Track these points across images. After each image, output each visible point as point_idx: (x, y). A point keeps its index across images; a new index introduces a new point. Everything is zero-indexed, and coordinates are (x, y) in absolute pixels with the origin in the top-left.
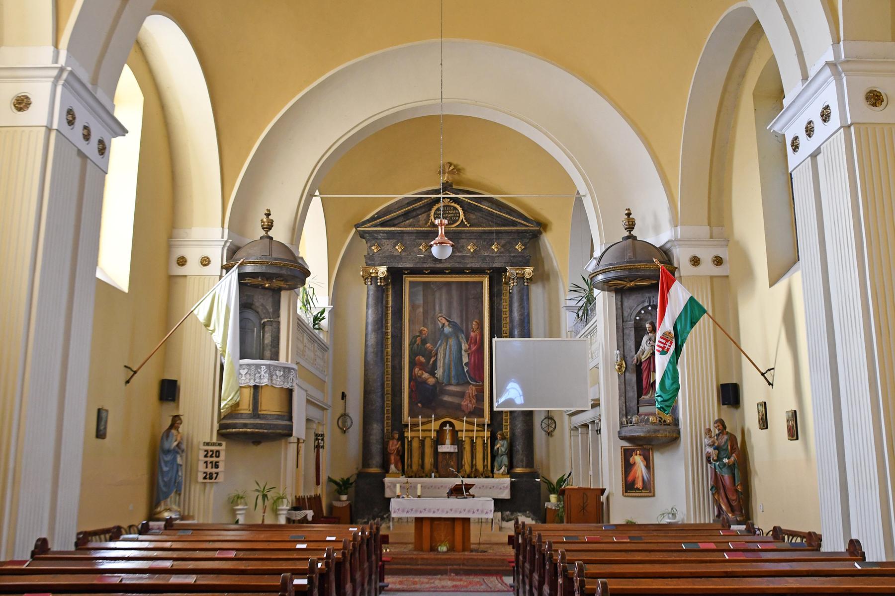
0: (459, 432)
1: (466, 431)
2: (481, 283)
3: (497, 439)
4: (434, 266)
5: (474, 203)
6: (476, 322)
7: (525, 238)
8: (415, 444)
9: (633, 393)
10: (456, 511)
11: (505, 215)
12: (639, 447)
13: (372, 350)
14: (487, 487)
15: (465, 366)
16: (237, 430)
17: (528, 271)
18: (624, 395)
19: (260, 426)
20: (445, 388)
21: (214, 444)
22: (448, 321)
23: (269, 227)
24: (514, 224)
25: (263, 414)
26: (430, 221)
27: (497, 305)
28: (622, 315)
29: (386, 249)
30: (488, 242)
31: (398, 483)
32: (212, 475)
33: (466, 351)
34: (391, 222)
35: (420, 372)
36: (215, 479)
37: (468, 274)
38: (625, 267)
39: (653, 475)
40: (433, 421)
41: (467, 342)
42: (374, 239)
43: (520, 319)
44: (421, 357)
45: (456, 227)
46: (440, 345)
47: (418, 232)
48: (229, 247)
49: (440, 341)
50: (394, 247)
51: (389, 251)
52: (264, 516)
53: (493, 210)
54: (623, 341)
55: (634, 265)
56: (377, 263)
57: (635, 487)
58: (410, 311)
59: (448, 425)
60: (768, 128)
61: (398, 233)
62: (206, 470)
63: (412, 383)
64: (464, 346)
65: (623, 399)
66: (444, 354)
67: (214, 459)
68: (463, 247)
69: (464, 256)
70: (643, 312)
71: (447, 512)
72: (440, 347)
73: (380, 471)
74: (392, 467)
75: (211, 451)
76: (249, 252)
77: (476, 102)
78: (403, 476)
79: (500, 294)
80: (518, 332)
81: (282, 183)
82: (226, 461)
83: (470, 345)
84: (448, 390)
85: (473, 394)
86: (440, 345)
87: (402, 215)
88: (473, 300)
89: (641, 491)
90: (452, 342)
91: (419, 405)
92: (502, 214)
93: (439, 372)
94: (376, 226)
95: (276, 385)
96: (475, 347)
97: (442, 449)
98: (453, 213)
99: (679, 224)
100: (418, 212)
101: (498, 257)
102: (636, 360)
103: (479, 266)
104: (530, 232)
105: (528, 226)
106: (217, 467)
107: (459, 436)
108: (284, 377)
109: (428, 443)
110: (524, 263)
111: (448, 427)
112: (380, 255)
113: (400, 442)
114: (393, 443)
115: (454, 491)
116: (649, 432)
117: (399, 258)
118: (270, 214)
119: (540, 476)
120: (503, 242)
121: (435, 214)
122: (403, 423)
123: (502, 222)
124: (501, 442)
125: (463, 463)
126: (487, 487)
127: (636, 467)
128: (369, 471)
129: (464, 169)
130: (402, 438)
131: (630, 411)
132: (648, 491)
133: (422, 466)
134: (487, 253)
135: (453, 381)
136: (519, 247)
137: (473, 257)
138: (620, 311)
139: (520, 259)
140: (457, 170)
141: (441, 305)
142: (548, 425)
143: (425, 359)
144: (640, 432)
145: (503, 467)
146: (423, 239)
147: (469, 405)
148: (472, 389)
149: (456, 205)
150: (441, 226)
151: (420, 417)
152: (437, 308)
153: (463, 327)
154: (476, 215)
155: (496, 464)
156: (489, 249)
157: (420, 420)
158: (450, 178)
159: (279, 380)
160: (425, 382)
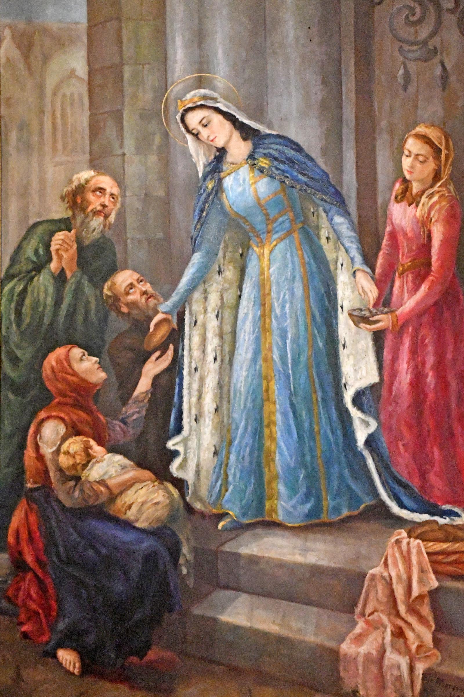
6: (426, 139)
15: (355, 413)
20: (228, 548)
44: (77, 352)
49: (197, 258)
66: (221, 336)
72: (197, 295)
84: (253, 560)
85: (415, 592)
96: (424, 288)
143: (102, 366)
148: (407, 559)
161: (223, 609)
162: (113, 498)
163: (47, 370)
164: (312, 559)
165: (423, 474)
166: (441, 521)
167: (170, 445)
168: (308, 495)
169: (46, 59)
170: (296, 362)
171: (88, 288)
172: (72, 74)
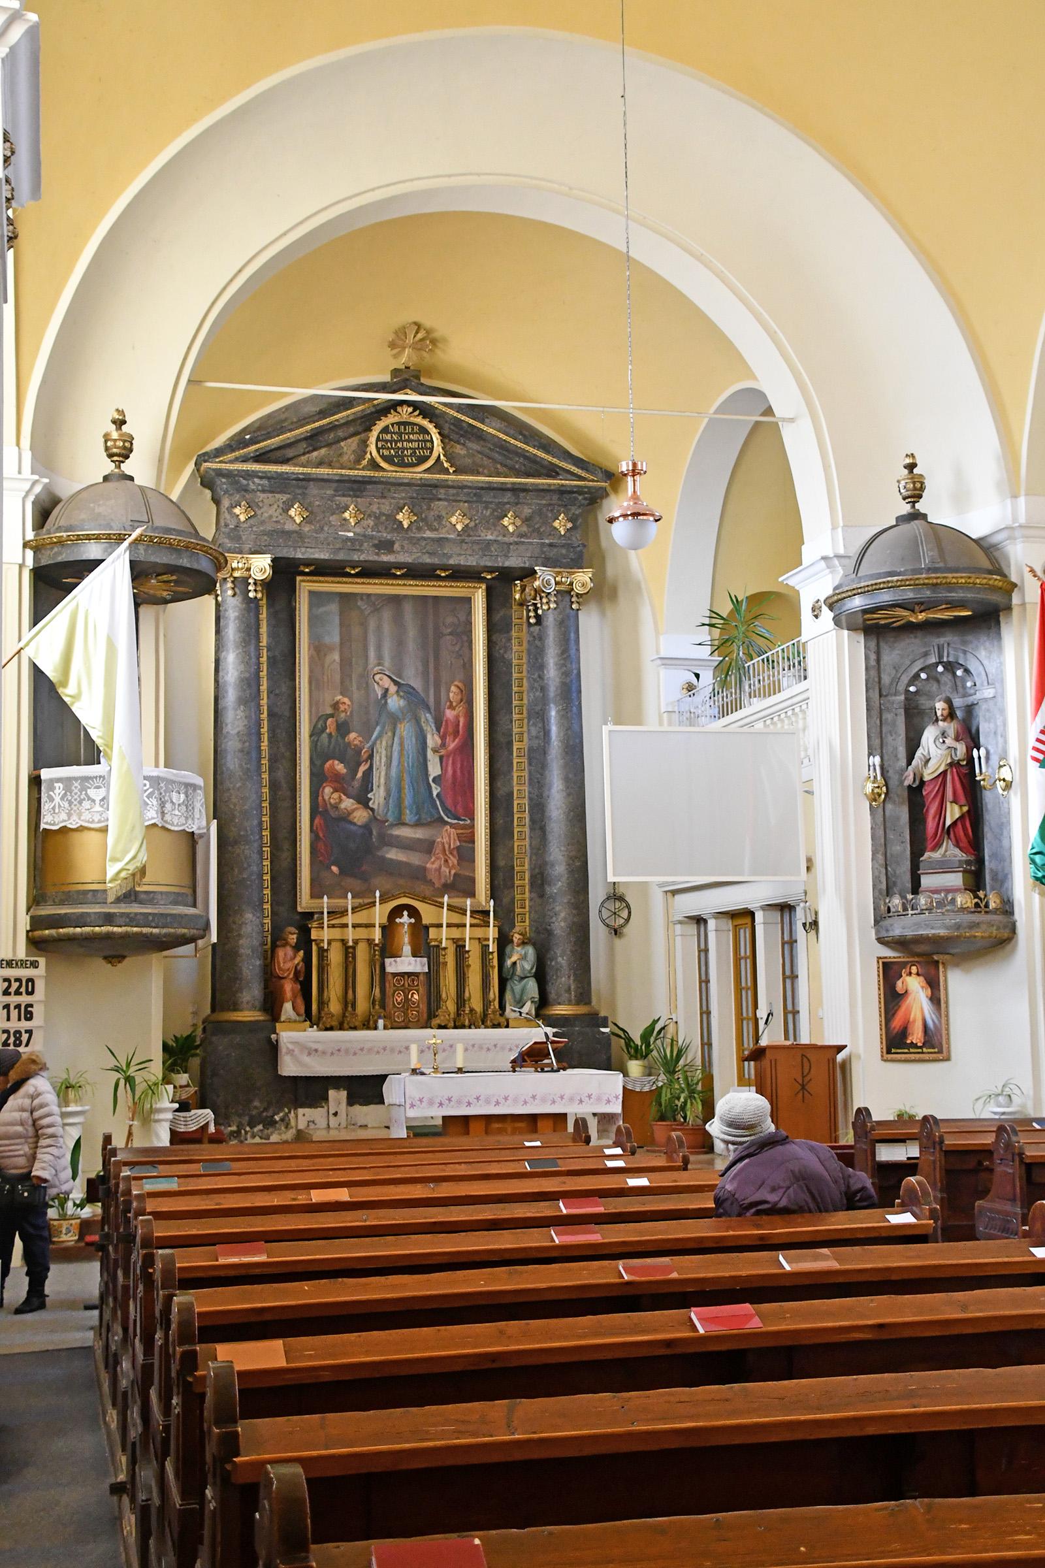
0: (431, 929)
1: (449, 925)
2: (468, 601)
3: (512, 941)
4: (376, 558)
5: (467, 419)
6: (458, 687)
7: (575, 505)
8: (335, 957)
9: (902, 848)
10: (544, 1100)
11: (535, 451)
12: (917, 959)
13: (239, 745)
14: (481, 1048)
15: (433, 785)
16: (87, 929)
17: (582, 579)
18: (882, 849)
19: (145, 920)
20: (389, 832)
21: (22, 964)
22: (396, 683)
23: (121, 452)
24: (553, 471)
25: (146, 892)
26: (368, 456)
27: (502, 651)
28: (880, 682)
29: (266, 515)
30: (494, 510)
31: (414, 1042)
32: (21, 1036)
33: (435, 751)
34: (278, 454)
35: (336, 795)
36: (27, 1045)
37: (357, 575)
38: (926, 581)
39: (947, 1016)
40: (378, 904)
41: (438, 730)
42: (238, 491)
43: (564, 684)
44: (336, 762)
45: (426, 471)
46: (380, 736)
47: (342, 481)
48: (37, 496)
49: (378, 728)
50: (286, 511)
51: (274, 519)
52: (131, 1126)
53: (508, 439)
54: (881, 737)
55: (944, 578)
56: (247, 547)
57: (909, 1042)
58: (311, 659)
59: (405, 913)
60: (780, 580)
61: (298, 479)
62: (7, 1025)
63: (317, 821)
64: (432, 740)
65: (880, 857)
67: (24, 999)
68: (439, 518)
69: (441, 538)
70: (923, 676)
71: (525, 1103)
72: (378, 742)
73: (262, 1018)
74: (288, 1007)
75: (16, 980)
76: (97, 511)
77: (571, 189)
78: (311, 1027)
79: (507, 627)
80: (558, 712)
81: (133, 348)
82: (47, 1003)
83: (443, 738)
84: (398, 836)
86: (380, 736)
87: (306, 439)
88: (451, 637)
89: (920, 1050)
90: (405, 730)
91: (334, 869)
92: (528, 448)
93: (377, 797)
94: (245, 460)
95: (172, 824)
96: (457, 740)
97: (392, 966)
98: (418, 441)
99: (1023, 492)
100: (340, 433)
101: (517, 543)
102: (911, 777)
103: (474, 564)
104: (586, 493)
105: (583, 479)
106: (29, 1016)
107: (431, 937)
108: (187, 806)
109: (362, 953)
110: (572, 559)
111: (405, 919)
112: (255, 529)
113: (301, 953)
114: (285, 955)
115: (529, 1057)
116: (958, 927)
117: (297, 537)
118: (124, 422)
119: (610, 1023)
120: (527, 511)
121: (378, 439)
122: (299, 909)
123: (524, 465)
124: (519, 949)
125: (467, 995)
126: (481, 1048)
127: (910, 999)
128: (235, 1018)
129: (445, 340)
130: (305, 942)
131: (895, 883)
132: (936, 1050)
133: (348, 1003)
134: (492, 534)
135: (408, 817)
136: (561, 524)
137: (463, 541)
138: (873, 673)
139: (564, 551)
140: (427, 340)
141: (379, 648)
142: (615, 913)
144: (939, 928)
145: (528, 1004)
146: (350, 496)
147: (443, 868)
149: (425, 423)
150: (633, 476)
151: (350, 895)
152: (372, 654)
153: (428, 695)
154: (468, 449)
155: (508, 996)
156: (494, 525)
157: (350, 902)
158: (415, 358)
159: (177, 812)
160: (345, 818)
161: (387, 853)
162: (349, 814)
163: (326, 769)
164: (418, 836)
165: (455, 807)
166: (461, 822)
167: (369, 796)
168: (416, 814)
169: (325, 655)
170: (413, 766)
171: (339, 738)
172: (334, 661)
